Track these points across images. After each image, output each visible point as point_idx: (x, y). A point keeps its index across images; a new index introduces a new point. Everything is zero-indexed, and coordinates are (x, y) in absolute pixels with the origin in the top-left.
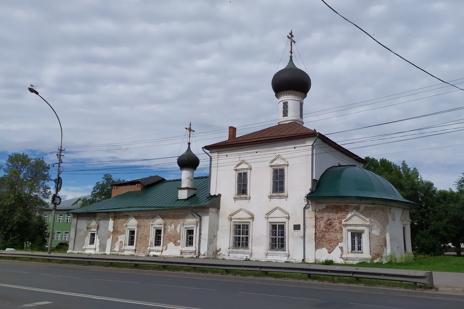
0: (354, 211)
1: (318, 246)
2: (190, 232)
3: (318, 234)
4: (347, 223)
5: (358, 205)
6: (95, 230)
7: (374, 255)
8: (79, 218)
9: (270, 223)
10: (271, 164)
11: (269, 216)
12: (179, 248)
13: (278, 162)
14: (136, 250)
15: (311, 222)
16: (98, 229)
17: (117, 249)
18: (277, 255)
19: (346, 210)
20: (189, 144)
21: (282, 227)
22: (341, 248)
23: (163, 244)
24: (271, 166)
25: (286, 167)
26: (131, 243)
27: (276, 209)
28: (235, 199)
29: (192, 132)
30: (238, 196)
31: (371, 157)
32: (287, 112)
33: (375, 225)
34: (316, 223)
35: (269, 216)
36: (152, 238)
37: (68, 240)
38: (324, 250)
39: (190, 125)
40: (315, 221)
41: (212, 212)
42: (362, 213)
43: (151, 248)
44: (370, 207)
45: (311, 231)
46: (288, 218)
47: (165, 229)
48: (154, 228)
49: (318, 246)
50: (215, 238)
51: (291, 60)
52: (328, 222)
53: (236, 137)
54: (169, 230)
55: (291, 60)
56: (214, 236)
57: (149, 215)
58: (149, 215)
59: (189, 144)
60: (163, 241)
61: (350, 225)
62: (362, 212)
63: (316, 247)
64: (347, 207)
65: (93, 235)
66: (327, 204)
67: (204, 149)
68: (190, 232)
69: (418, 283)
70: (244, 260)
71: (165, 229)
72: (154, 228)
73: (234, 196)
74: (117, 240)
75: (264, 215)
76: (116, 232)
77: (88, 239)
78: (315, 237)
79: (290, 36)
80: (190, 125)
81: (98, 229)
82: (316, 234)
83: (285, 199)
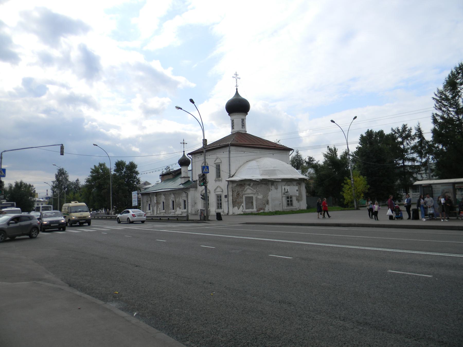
0: (248, 186)
1: (234, 206)
2: (185, 201)
3: (234, 200)
4: (245, 193)
5: (249, 183)
6: (150, 202)
7: (259, 209)
8: (143, 196)
9: (217, 195)
10: (215, 162)
11: (216, 191)
12: (181, 210)
13: (218, 161)
14: (165, 212)
15: (230, 193)
16: (151, 202)
17: (158, 212)
18: (54, 218)
19: (245, 186)
20: (184, 152)
21: (221, 196)
22: (243, 206)
23: (175, 209)
24: (215, 163)
25: (221, 164)
26: (164, 209)
27: (218, 187)
28: (216, 181)
29: (185, 144)
30: (217, 179)
31: (376, 129)
32: (234, 126)
33: (259, 193)
34: (232, 194)
35: (216, 191)
36: (171, 206)
37: (457, 187)
38: (236, 208)
39: (184, 140)
40: (232, 192)
41: (192, 190)
42: (252, 187)
43: (171, 211)
44: (256, 184)
45: (230, 198)
46: (222, 191)
47: (175, 201)
48: (172, 200)
49: (234, 206)
50: (196, 204)
51: (237, 91)
52: (238, 193)
53: (207, 145)
54: (177, 201)
55: (237, 91)
56: (195, 203)
57: (169, 193)
58: (169, 193)
59: (184, 152)
60: (175, 207)
61: (246, 194)
62: (252, 186)
63: (233, 207)
64: (245, 184)
65: (149, 204)
66: (237, 183)
67: (188, 155)
68: (185, 201)
69: (141, 223)
70: (193, 215)
71: (175, 201)
72: (172, 200)
73: (214, 179)
74: (158, 207)
75: (214, 191)
76: (158, 203)
77: (148, 208)
78: (233, 201)
79: (235, 76)
80: (184, 140)
81: (151, 202)
82: (233, 199)
83: (221, 182)
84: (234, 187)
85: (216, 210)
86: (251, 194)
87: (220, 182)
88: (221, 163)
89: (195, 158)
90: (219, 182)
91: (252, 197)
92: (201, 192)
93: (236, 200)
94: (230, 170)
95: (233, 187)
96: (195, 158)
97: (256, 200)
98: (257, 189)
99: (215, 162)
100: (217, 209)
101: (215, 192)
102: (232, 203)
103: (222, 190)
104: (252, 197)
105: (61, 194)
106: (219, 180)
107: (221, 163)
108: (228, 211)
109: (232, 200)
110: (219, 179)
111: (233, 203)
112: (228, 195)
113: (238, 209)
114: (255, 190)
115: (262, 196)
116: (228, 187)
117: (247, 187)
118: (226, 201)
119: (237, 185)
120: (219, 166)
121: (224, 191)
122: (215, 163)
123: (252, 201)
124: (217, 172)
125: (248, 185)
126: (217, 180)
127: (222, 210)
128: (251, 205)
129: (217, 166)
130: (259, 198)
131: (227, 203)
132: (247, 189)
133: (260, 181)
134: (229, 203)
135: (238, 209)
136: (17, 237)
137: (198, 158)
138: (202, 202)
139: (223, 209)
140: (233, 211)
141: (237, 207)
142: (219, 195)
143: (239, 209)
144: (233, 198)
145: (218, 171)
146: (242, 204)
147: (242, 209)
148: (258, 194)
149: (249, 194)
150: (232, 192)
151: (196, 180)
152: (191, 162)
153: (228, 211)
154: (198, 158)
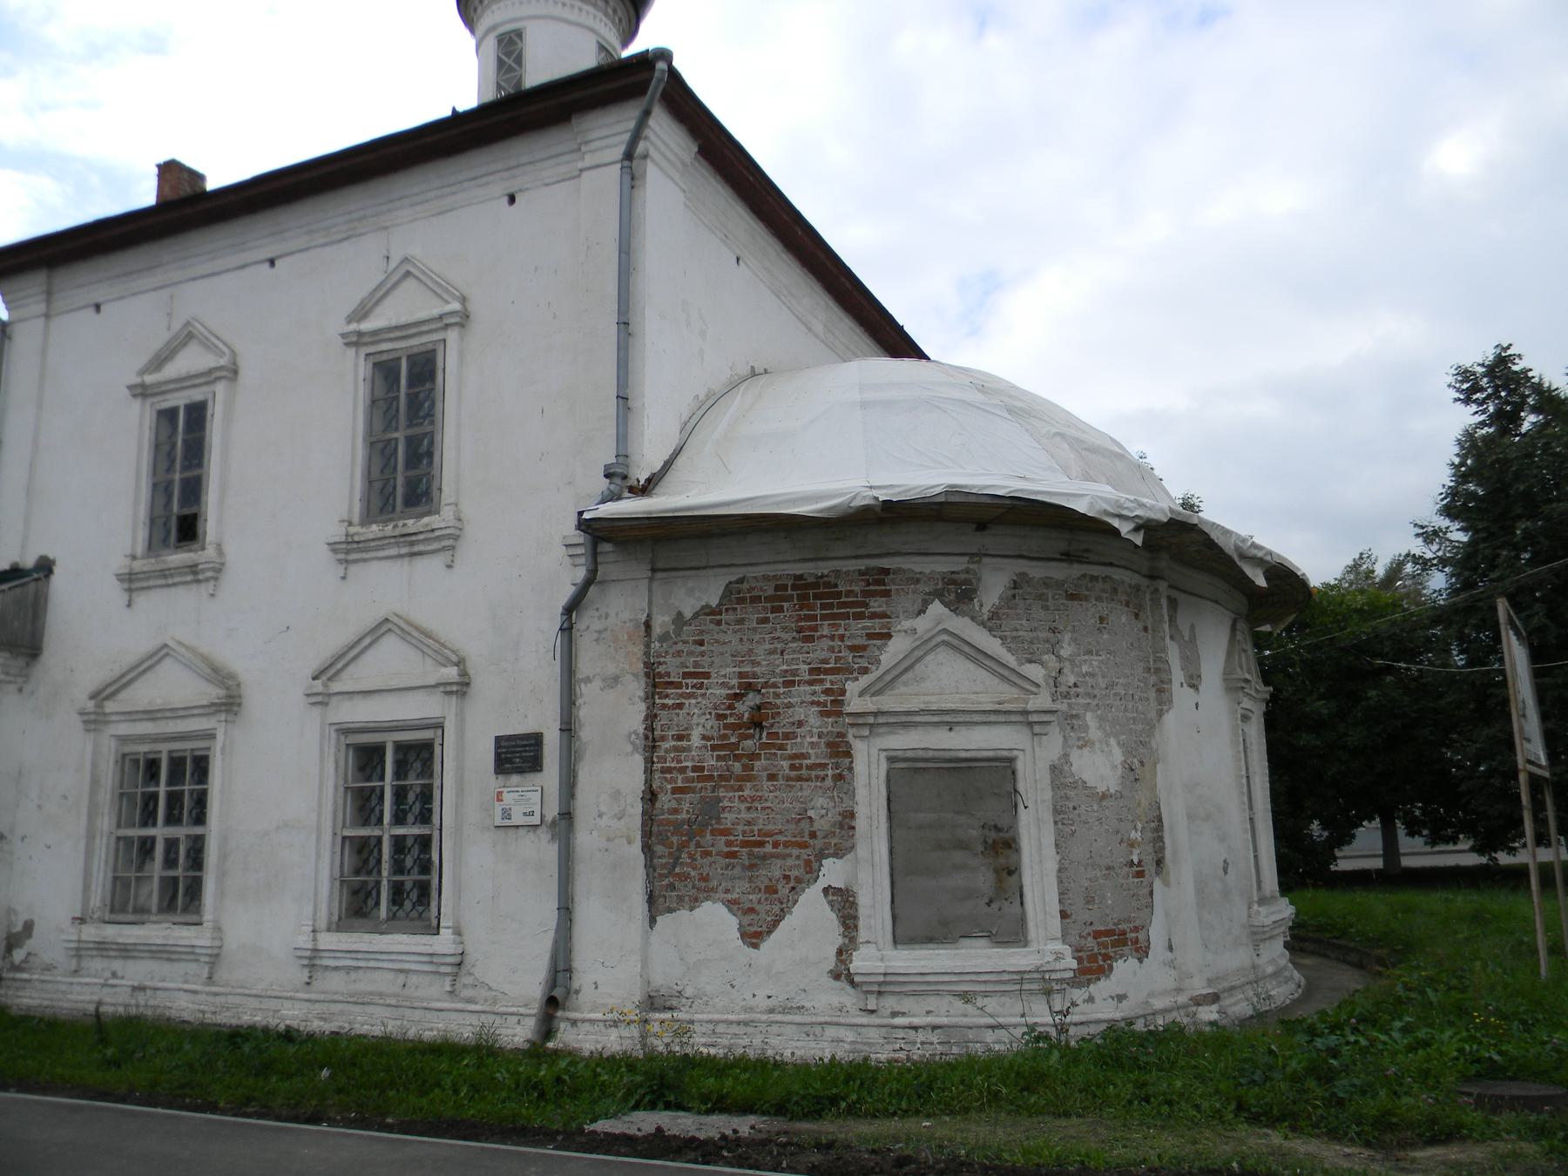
0: (937, 608)
4: (888, 702)
5: (958, 564)
7: (1090, 942)
9: (345, 731)
10: (354, 326)
11: (336, 687)
22: (844, 903)
27: (382, 628)
34: (651, 718)
35: (336, 687)
40: (649, 697)
42: (992, 623)
44: (1046, 583)
46: (461, 688)
61: (906, 720)
62: (994, 615)
63: (651, 899)
64: (878, 581)
73: (120, 563)
78: (648, 819)
82: (650, 796)
84: (679, 619)
85: (328, 941)
86: (996, 716)
87: (435, 564)
88: (462, 325)
89: (47, 316)
90: (405, 564)
91: (1003, 767)
92: (93, 697)
93: (711, 809)
94: (622, 398)
95: (661, 622)
96: (47, 316)
97: (1059, 812)
98: (1065, 652)
99: (366, 326)
100: (338, 926)
101: (320, 700)
102: (636, 848)
103: (460, 663)
104: (1003, 767)
105: (822, 677)
106: (412, 547)
107: (462, 325)
108: (561, 969)
109: (638, 808)
110: (412, 525)
111: (647, 849)
112: (568, 728)
113: (753, 938)
114: (1034, 672)
115: (1118, 756)
116: (567, 630)
117: (923, 624)
118: (517, 819)
119: (728, 591)
120: (425, 369)
121: (485, 684)
122: (355, 341)
123: (1003, 822)
124: (161, 489)
125: (939, 594)
126: (148, 575)
127: (443, 942)
128: (983, 880)
129: (385, 371)
130: (1090, 777)
131: (545, 850)
132: (926, 647)
133: (1138, 539)
134: (585, 839)
135: (753, 938)
136: (457, 293)
137: (98, 307)
138: (91, 836)
139: (458, 932)
140: (645, 963)
141: (731, 904)
142: (390, 739)
143: (766, 946)
144: (649, 771)
145: (399, 435)
146: (833, 872)
147: (833, 936)
148: (1071, 721)
149: (950, 719)
150: (637, 688)
151: (29, 562)
152: (649, 93)
153: (561, 969)
154: (98, 307)
